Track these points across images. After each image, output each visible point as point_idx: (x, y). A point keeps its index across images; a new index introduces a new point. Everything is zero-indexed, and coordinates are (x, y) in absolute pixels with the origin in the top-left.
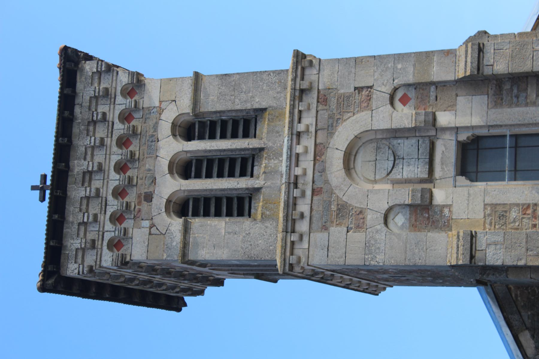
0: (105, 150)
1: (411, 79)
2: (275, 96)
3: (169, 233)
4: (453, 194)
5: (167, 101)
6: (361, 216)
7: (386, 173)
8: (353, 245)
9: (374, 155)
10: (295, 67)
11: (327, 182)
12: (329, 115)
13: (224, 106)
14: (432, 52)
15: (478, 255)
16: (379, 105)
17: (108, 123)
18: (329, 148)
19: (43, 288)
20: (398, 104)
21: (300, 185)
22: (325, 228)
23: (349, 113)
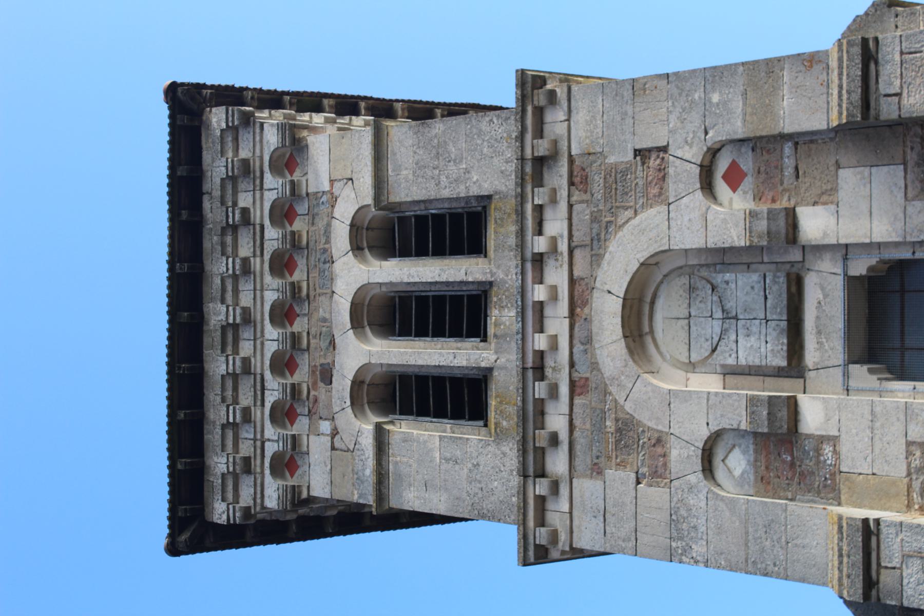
0: (252, 282)
1: (738, 128)
2: (503, 168)
3: (358, 450)
4: (839, 412)
5: (340, 180)
6: (659, 450)
7: (710, 349)
8: (648, 515)
9: (686, 305)
10: (520, 108)
11: (595, 366)
12: (592, 213)
13: (424, 191)
14: (779, 60)
15: (886, 579)
16: (680, 191)
17: (254, 229)
18: (595, 290)
19: (173, 550)
20: (722, 188)
21: (548, 372)
22: (597, 471)
23: (627, 209)
